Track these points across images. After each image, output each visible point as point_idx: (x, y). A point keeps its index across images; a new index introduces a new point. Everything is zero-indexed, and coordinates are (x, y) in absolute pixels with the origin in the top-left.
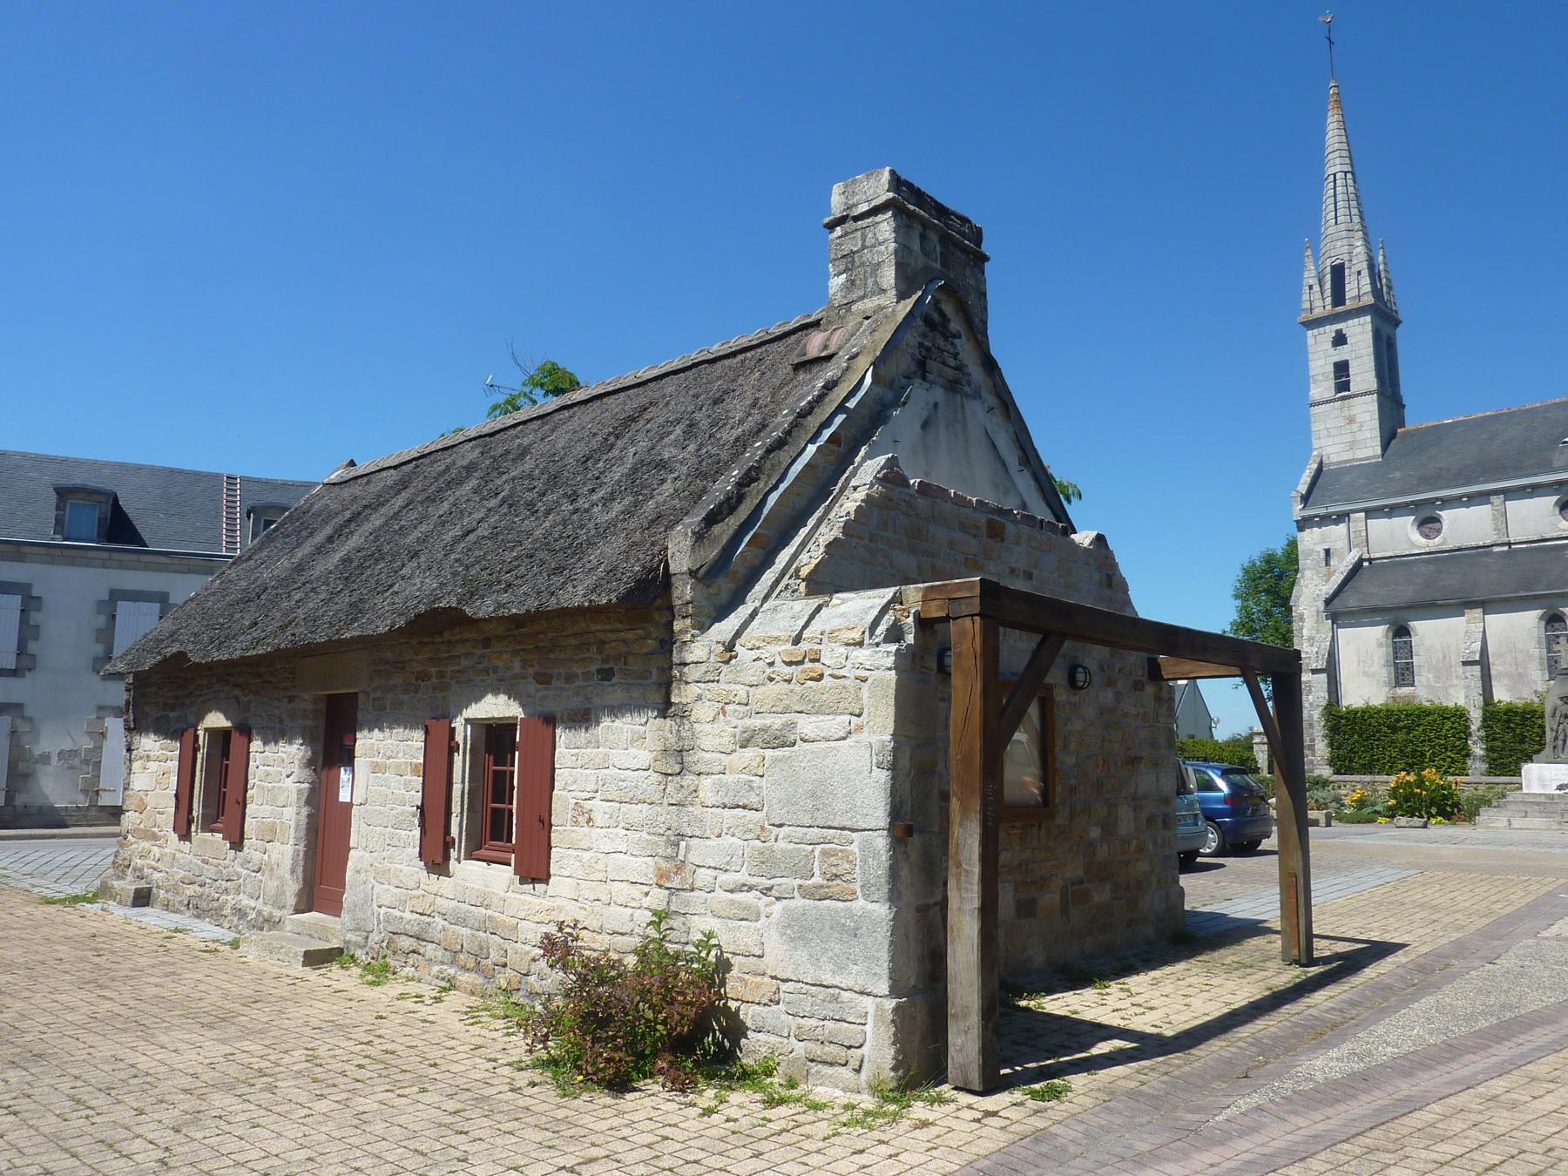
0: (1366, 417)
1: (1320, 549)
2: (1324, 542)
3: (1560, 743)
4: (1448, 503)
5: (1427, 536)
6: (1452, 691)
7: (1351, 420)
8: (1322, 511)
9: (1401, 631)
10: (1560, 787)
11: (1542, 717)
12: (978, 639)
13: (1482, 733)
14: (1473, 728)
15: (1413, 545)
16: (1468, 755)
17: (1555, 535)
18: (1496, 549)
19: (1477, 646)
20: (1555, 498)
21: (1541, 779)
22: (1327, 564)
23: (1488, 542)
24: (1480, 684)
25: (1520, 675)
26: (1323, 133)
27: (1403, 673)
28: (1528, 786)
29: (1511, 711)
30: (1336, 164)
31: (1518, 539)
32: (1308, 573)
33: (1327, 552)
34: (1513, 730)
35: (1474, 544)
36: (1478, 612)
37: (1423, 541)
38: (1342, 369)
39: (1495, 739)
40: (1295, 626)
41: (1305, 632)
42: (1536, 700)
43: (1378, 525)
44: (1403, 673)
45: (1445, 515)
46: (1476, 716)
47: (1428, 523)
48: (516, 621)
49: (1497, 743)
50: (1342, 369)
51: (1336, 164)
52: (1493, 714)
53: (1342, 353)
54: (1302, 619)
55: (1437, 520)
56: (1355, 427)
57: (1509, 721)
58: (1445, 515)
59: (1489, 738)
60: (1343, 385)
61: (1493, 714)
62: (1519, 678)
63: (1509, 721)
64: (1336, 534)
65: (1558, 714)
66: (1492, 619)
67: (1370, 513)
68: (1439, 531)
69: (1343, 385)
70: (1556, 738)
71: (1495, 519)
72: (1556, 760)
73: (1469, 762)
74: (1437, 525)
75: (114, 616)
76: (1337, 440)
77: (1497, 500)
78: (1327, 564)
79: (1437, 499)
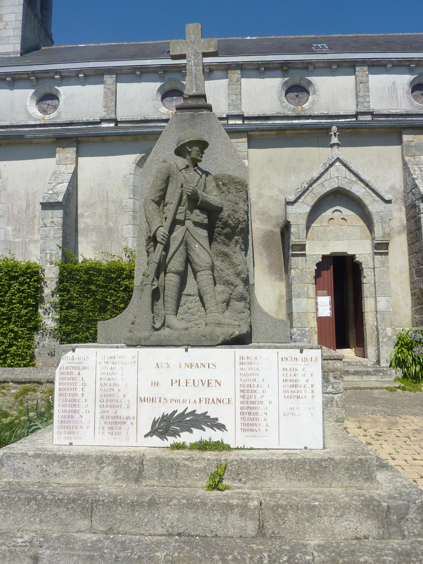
0: (12, 17)
3: (171, 280)
4: (67, 78)
5: (44, 112)
10: (165, 426)
11: (131, 277)
13: (56, 299)
14: (47, 291)
15: (30, 116)
16: (36, 328)
17: (156, 117)
18: (104, 125)
19: (63, 187)
20: (158, 85)
21: (109, 399)
23: (97, 119)
24: (60, 234)
25: (110, 230)
28: (70, 426)
29: (93, 271)
31: (124, 118)
34: (94, 293)
35: (84, 119)
36: (70, 152)
37: (40, 115)
39: (70, 307)
42: (125, 259)
45: (64, 91)
46: (51, 275)
47: (47, 98)
49: (73, 312)
52: (73, 275)
55: (54, 97)
57: (89, 282)
58: (64, 91)
59: (65, 305)
61: (73, 275)
62: (108, 233)
63: (89, 282)
65: (172, 197)
66: (85, 162)
68: (55, 108)
70: (162, 268)
71: (106, 96)
72: (155, 338)
73: (37, 338)
74: (55, 102)
75: (292, 348)
77: (109, 79)
79: (57, 72)
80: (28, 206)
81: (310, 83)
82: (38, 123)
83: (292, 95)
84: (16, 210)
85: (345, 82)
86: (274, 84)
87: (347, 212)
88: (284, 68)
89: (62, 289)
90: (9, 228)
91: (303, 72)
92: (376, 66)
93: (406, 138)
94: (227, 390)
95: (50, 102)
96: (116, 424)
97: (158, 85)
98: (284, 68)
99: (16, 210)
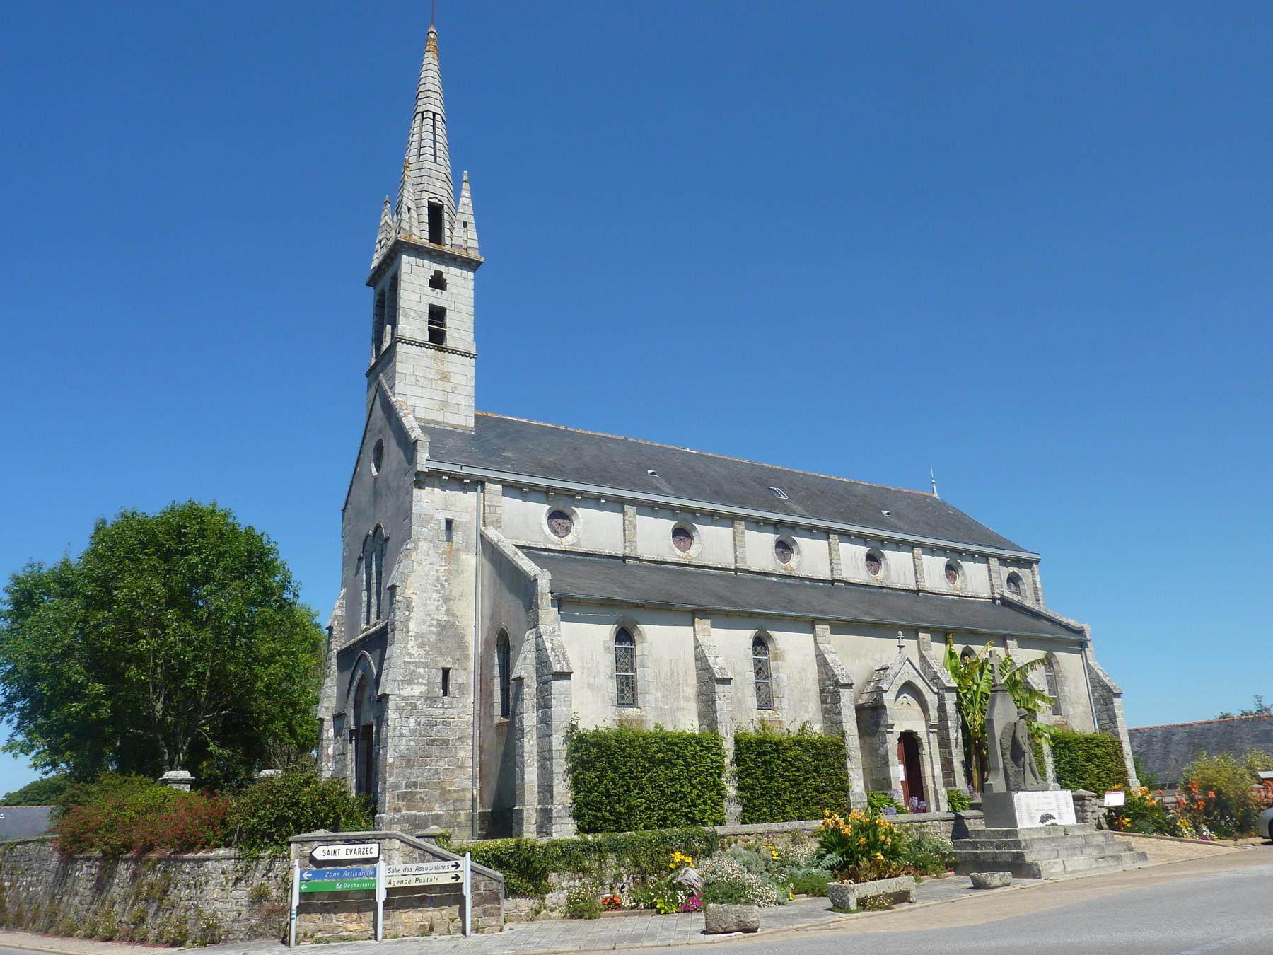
0: (461, 380)
1: (442, 516)
2: (447, 508)
5: (556, 532)
6: (679, 715)
7: (445, 377)
8: (455, 469)
9: (625, 636)
12: (447, 225)
14: (727, 761)
20: (673, 523)
22: (449, 539)
25: (739, 700)
26: (418, 67)
27: (627, 690)
30: (432, 101)
32: (423, 546)
33: (449, 523)
38: (437, 315)
40: (399, 615)
41: (412, 626)
43: (512, 507)
44: (627, 690)
47: (560, 518)
48: (551, 786)
50: (437, 315)
51: (432, 101)
53: (438, 298)
54: (409, 606)
56: (448, 386)
60: (437, 337)
64: (463, 503)
67: (512, 489)
68: (568, 530)
69: (437, 337)
74: (566, 522)
76: (427, 393)
78: (449, 539)
80: (673, 673)
81: (795, 542)
82: (558, 548)
83: (780, 550)
84: (662, 676)
85: (820, 545)
86: (769, 538)
87: (911, 699)
88: (776, 526)
89: (738, 760)
90: (659, 694)
91: (790, 531)
92: (846, 536)
93: (921, 635)
94: (1054, 806)
95: (560, 521)
96: (1031, 819)
97: (673, 523)
98: (776, 526)
99: (662, 676)
